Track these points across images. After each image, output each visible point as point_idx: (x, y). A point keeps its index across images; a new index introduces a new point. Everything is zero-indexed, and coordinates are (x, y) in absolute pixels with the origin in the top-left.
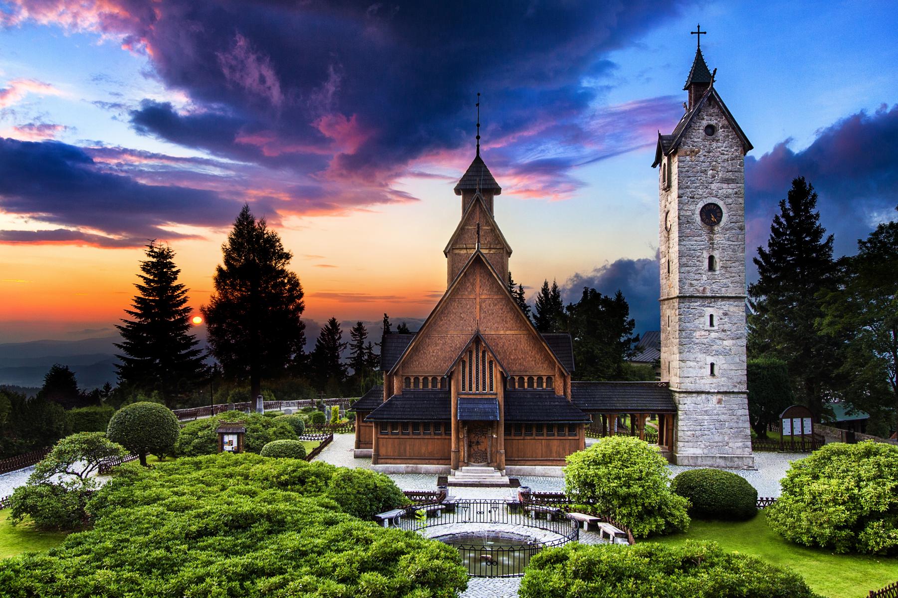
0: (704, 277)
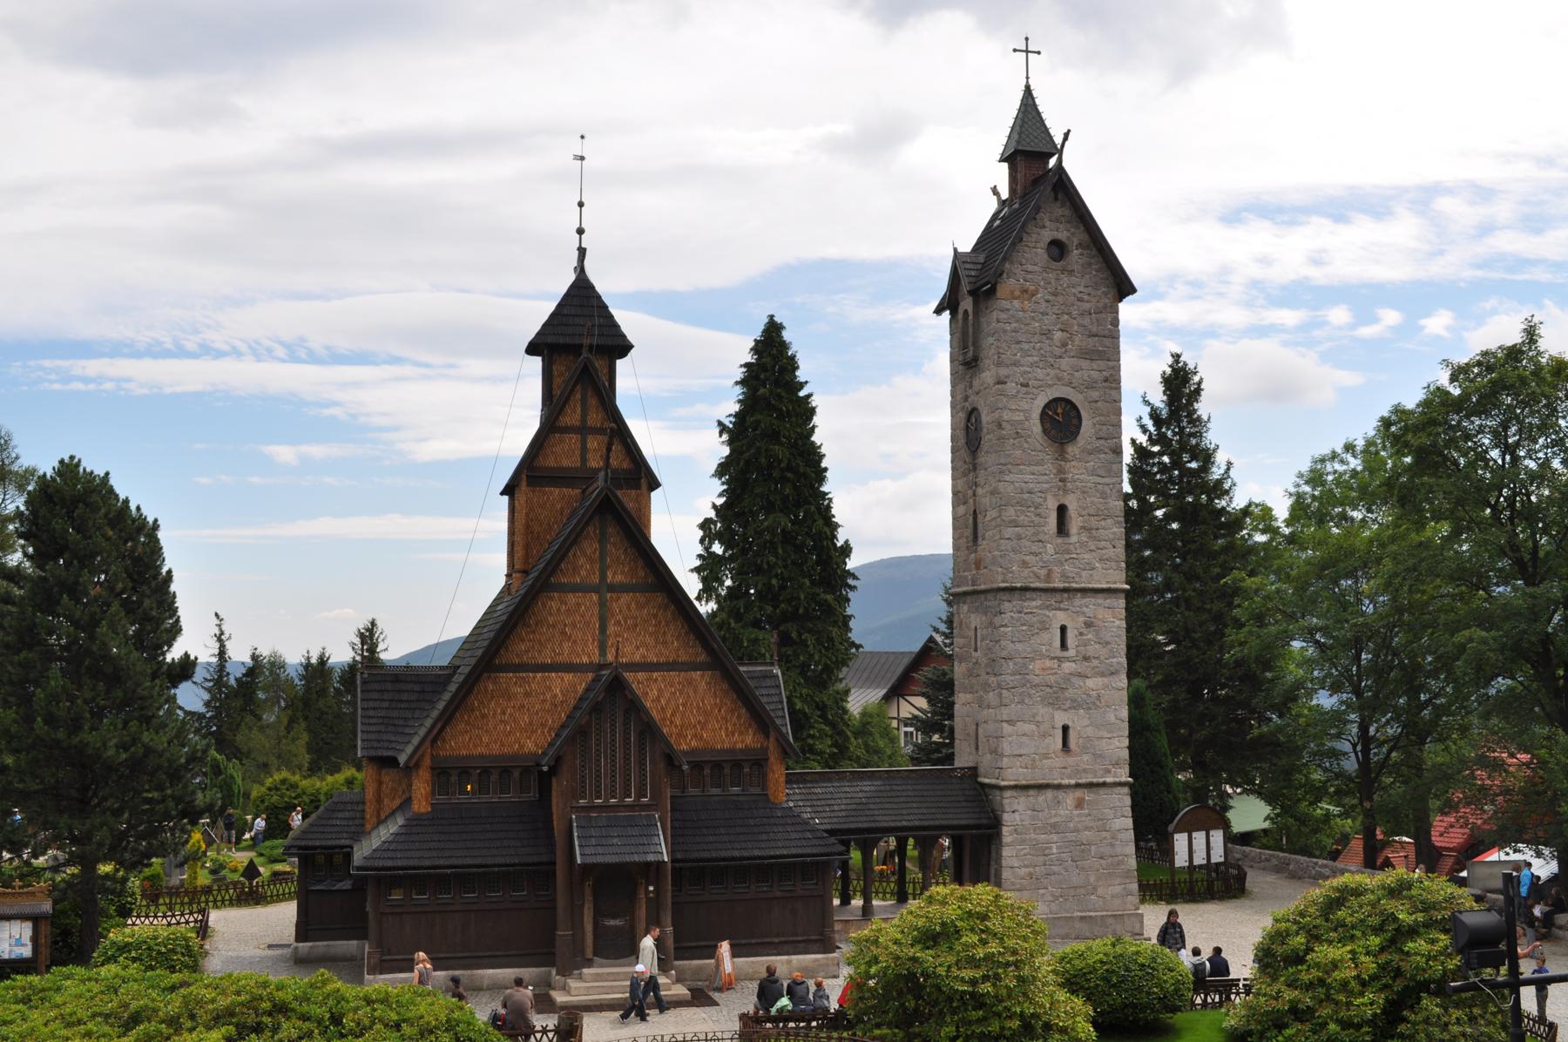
0: (1050, 548)
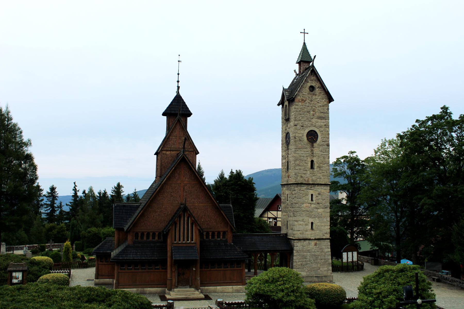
0: (308, 172)
